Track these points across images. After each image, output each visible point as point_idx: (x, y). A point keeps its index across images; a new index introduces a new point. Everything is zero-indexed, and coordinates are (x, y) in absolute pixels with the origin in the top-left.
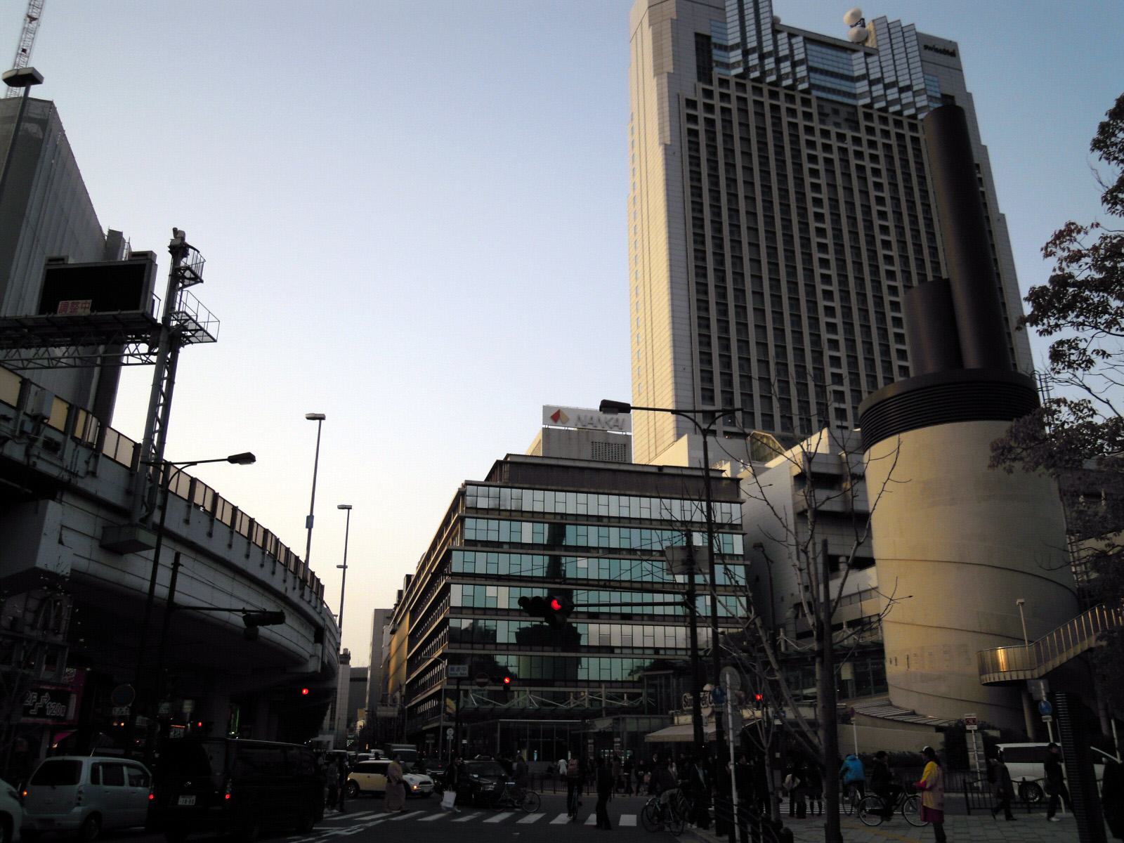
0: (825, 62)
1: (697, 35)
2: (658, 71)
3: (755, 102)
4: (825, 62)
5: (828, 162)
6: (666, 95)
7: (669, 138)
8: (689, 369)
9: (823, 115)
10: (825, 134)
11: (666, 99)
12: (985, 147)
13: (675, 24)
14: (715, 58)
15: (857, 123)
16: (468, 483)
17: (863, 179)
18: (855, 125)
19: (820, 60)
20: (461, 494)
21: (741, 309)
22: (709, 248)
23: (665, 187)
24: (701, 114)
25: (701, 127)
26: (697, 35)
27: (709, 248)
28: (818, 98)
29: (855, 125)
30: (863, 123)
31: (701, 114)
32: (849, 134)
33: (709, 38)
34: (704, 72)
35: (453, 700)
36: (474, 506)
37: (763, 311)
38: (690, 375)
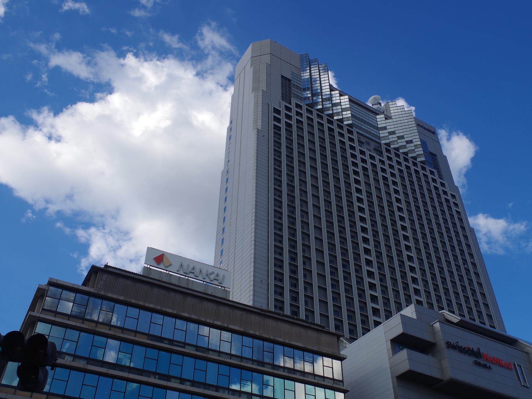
0: (361, 114)
1: (283, 77)
2: (255, 89)
3: (318, 122)
4: (361, 114)
5: (365, 169)
6: (260, 102)
7: (260, 126)
8: (265, 282)
9: (361, 143)
10: (362, 153)
11: (260, 104)
12: (445, 157)
13: (269, 67)
14: (293, 91)
15: (382, 153)
16: (51, 284)
17: (387, 186)
18: (381, 153)
19: (358, 113)
20: (40, 294)
21: (305, 235)
22: (284, 179)
23: (255, 167)
24: (282, 117)
25: (283, 126)
26: (283, 77)
27: (284, 179)
28: (357, 132)
29: (381, 153)
30: (385, 154)
31: (282, 117)
32: (377, 157)
33: (290, 81)
34: (286, 96)
35: (173, 34)
36: (54, 309)
37: (325, 290)
38: (266, 287)
